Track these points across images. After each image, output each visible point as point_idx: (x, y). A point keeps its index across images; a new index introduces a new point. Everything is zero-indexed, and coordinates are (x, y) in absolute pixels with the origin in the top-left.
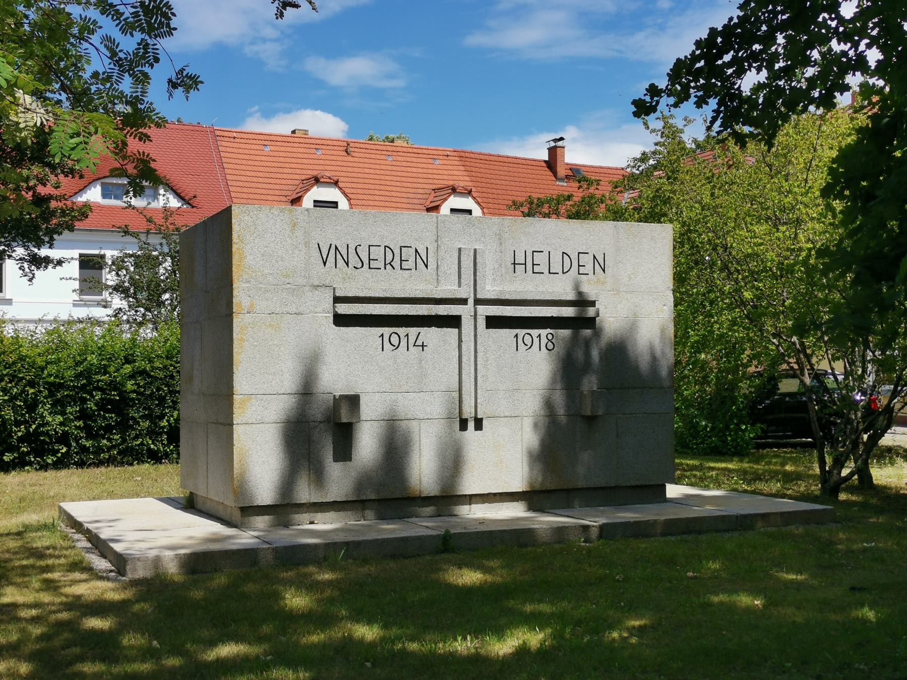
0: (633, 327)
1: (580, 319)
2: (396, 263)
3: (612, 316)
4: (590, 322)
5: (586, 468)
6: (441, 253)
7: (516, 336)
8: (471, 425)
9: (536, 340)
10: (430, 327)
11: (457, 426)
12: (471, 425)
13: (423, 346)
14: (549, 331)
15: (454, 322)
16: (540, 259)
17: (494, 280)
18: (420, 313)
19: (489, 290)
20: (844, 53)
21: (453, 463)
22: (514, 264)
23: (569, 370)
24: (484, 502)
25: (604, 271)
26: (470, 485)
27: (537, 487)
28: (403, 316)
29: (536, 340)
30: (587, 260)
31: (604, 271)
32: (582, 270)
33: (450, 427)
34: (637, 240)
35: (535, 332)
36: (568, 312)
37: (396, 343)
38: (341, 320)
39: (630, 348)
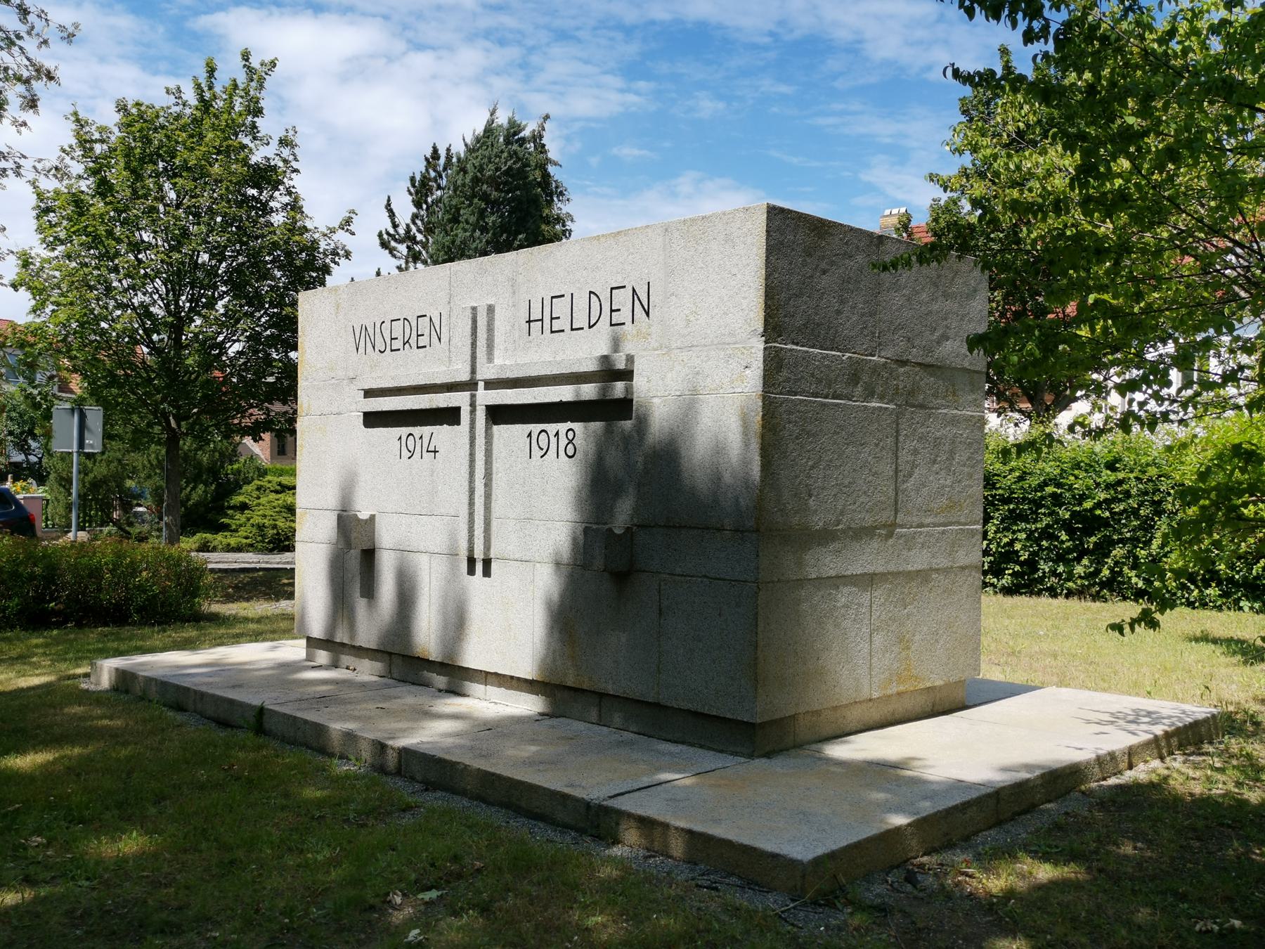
0: (689, 407)
1: (606, 403)
2: (413, 341)
3: (656, 389)
4: (624, 407)
5: (616, 668)
6: (453, 319)
7: (530, 435)
8: (479, 567)
9: (553, 440)
10: (441, 424)
11: (464, 566)
12: (479, 567)
13: (435, 452)
14: (569, 425)
15: (450, 416)
16: (561, 308)
17: (506, 350)
18: (443, 405)
19: (504, 363)
20: (1087, 125)
21: (456, 623)
22: (529, 322)
23: (599, 487)
24: (500, 686)
25: (648, 314)
26: (473, 657)
27: (547, 680)
28: (408, 411)
29: (553, 440)
30: (623, 298)
31: (648, 314)
32: (616, 318)
33: (454, 568)
34: (701, 248)
35: (552, 428)
36: (589, 391)
37: (544, 444)
38: (373, 420)
39: (683, 453)
